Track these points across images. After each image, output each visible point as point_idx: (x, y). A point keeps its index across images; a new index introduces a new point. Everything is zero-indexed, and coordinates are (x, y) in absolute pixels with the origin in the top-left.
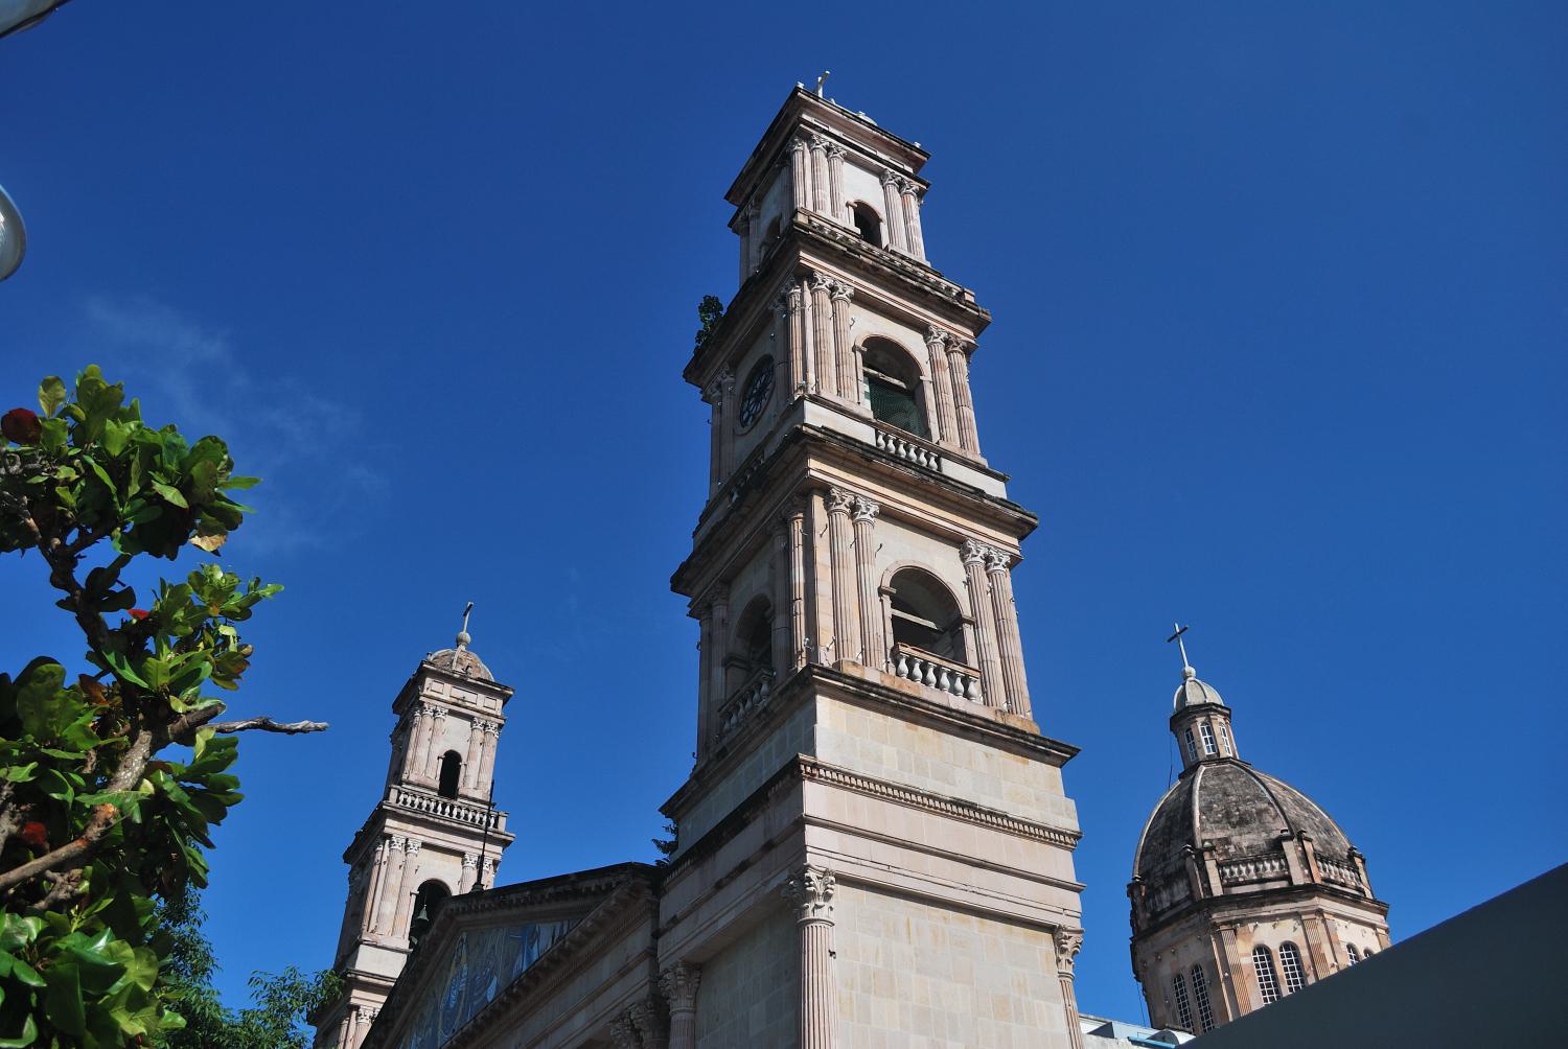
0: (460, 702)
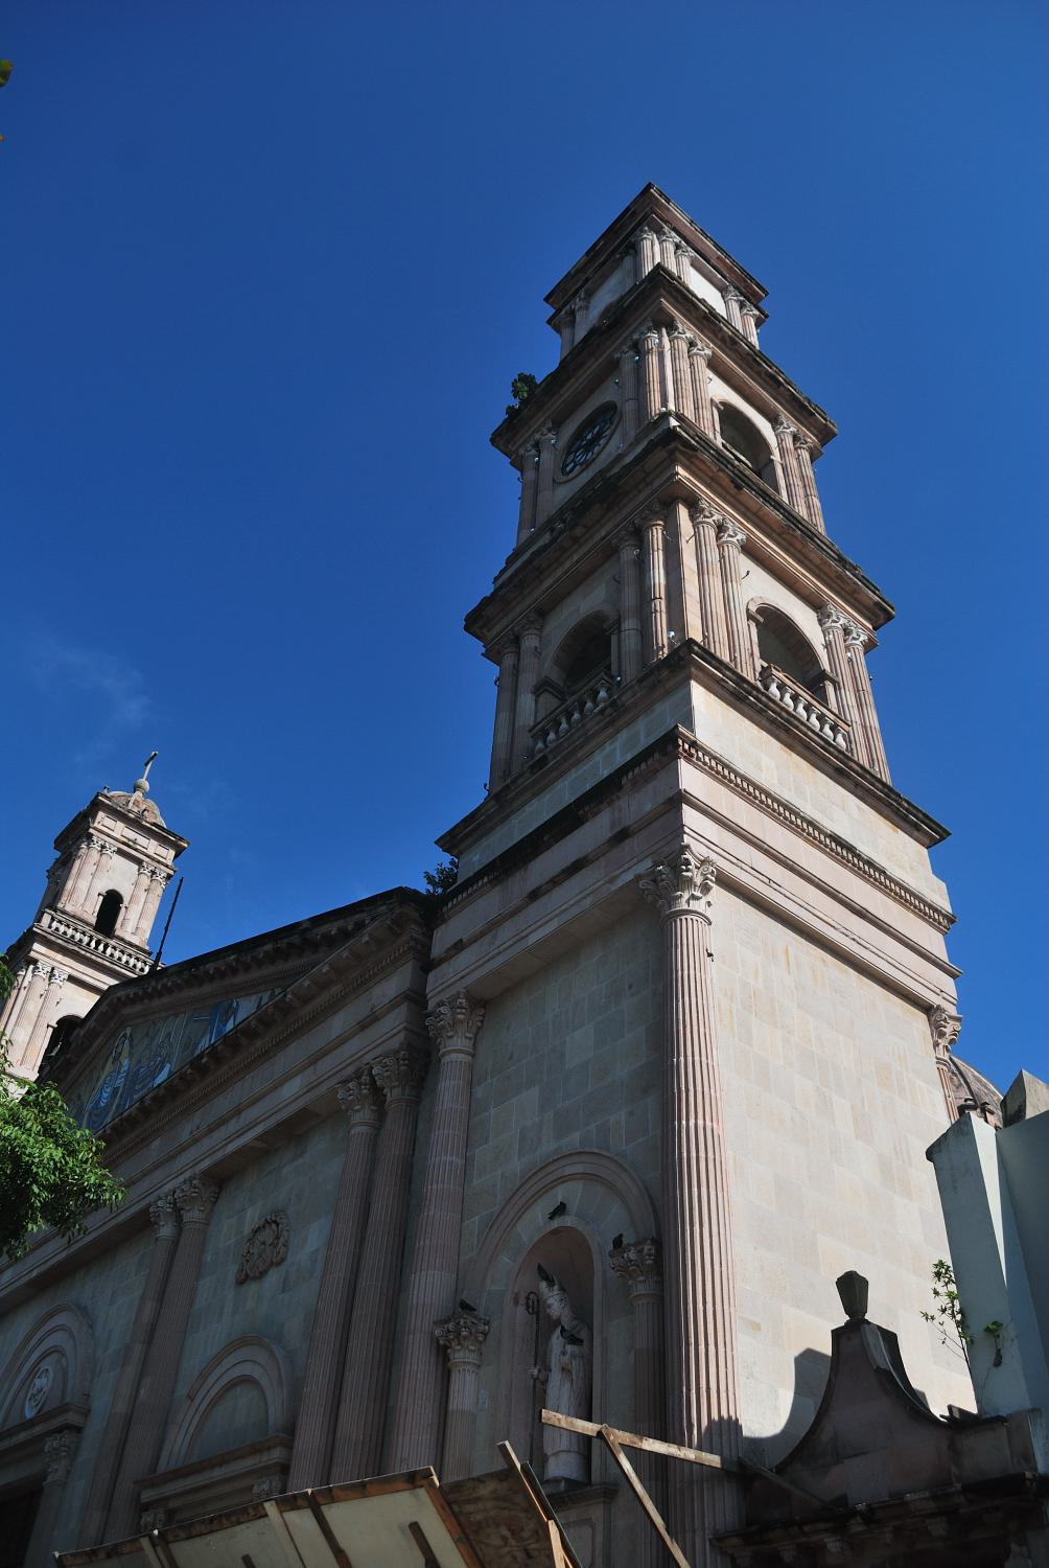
0: (131, 843)
